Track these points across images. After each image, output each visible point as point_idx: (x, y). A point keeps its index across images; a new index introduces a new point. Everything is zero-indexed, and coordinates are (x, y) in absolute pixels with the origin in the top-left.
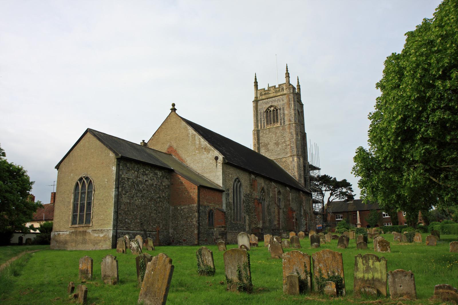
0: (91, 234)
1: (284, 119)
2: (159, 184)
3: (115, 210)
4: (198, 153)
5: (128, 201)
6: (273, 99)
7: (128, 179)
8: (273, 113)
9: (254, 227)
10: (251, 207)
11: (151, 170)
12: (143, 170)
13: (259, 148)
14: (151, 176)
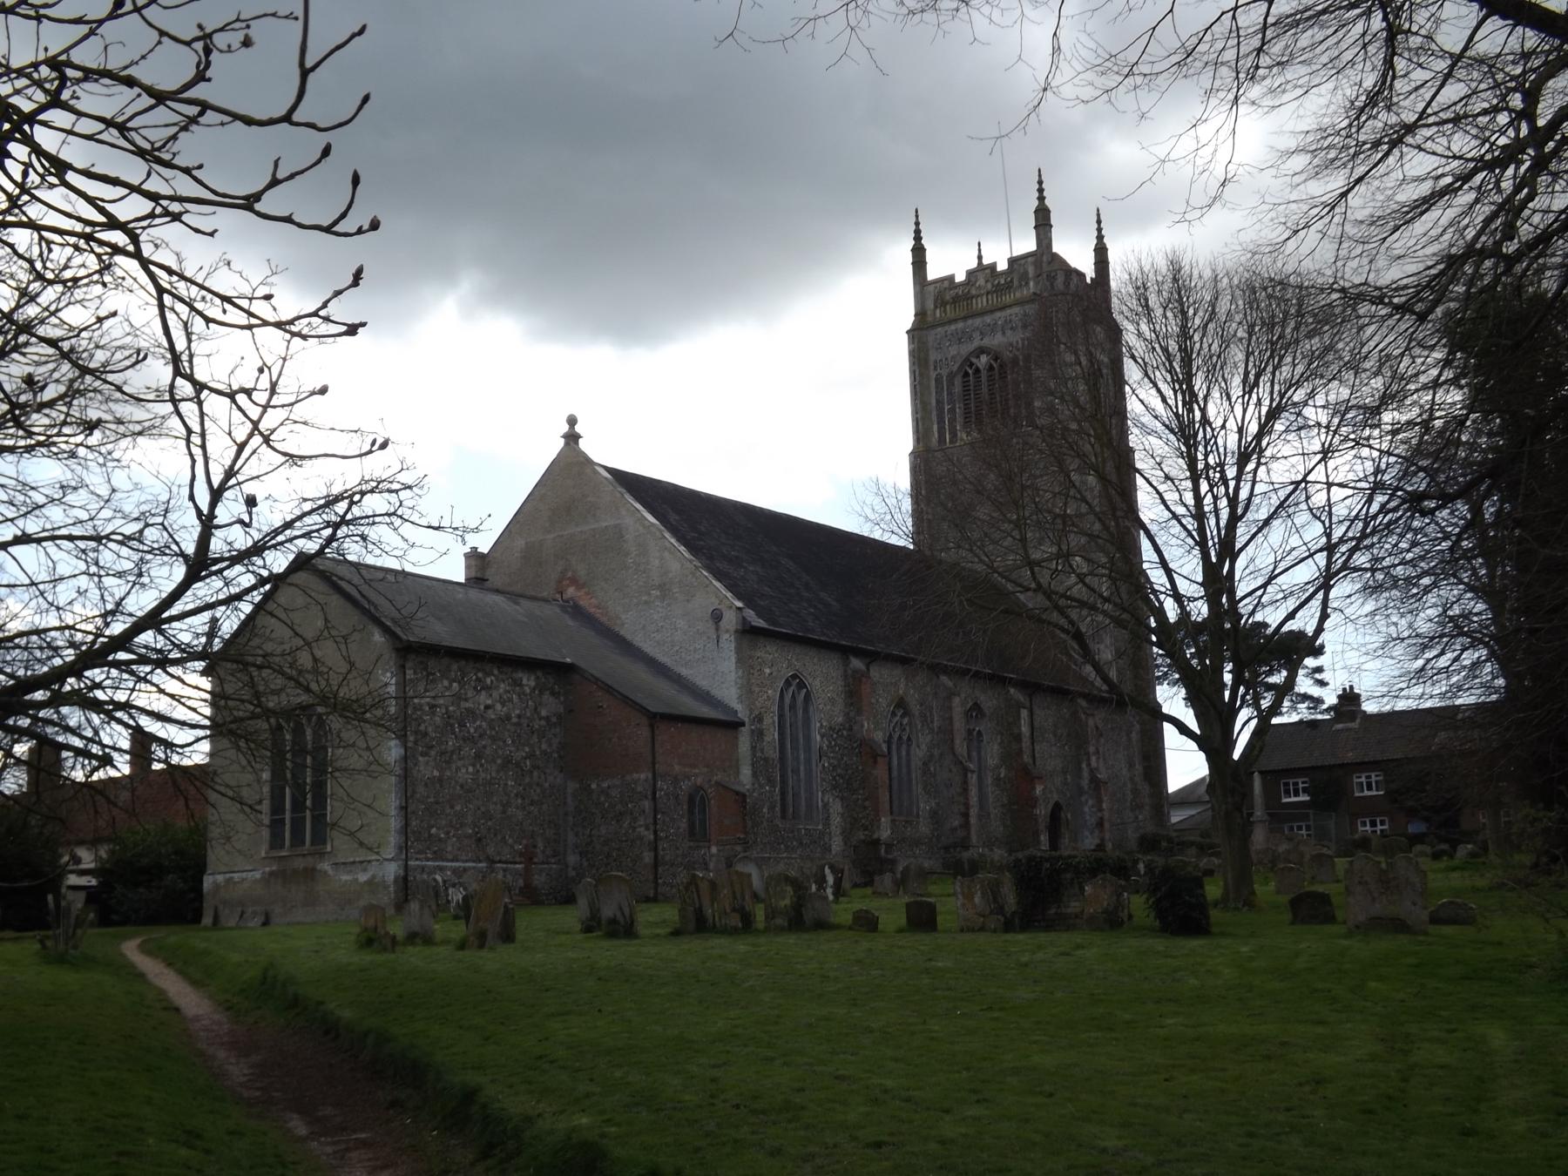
0: (329, 876)
2: (528, 714)
3: (398, 802)
4: (657, 597)
5: (436, 773)
6: (988, 319)
7: (433, 707)
8: (990, 379)
9: (862, 837)
10: (850, 772)
11: (501, 673)
12: (475, 674)
14: (501, 691)
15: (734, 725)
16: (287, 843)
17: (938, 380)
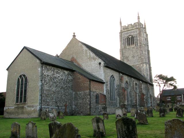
1: (137, 42)
6: (131, 31)
7: (48, 75)
8: (131, 39)
13: (123, 60)
15: (104, 83)
16: (19, 102)
17: (124, 39)
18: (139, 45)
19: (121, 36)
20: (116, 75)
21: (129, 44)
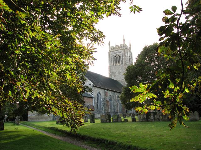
1: (123, 61)
6: (118, 51)
8: (118, 58)
13: (111, 77)
17: (112, 58)
18: (124, 63)
19: (109, 55)
20: (102, 92)
21: (116, 62)
